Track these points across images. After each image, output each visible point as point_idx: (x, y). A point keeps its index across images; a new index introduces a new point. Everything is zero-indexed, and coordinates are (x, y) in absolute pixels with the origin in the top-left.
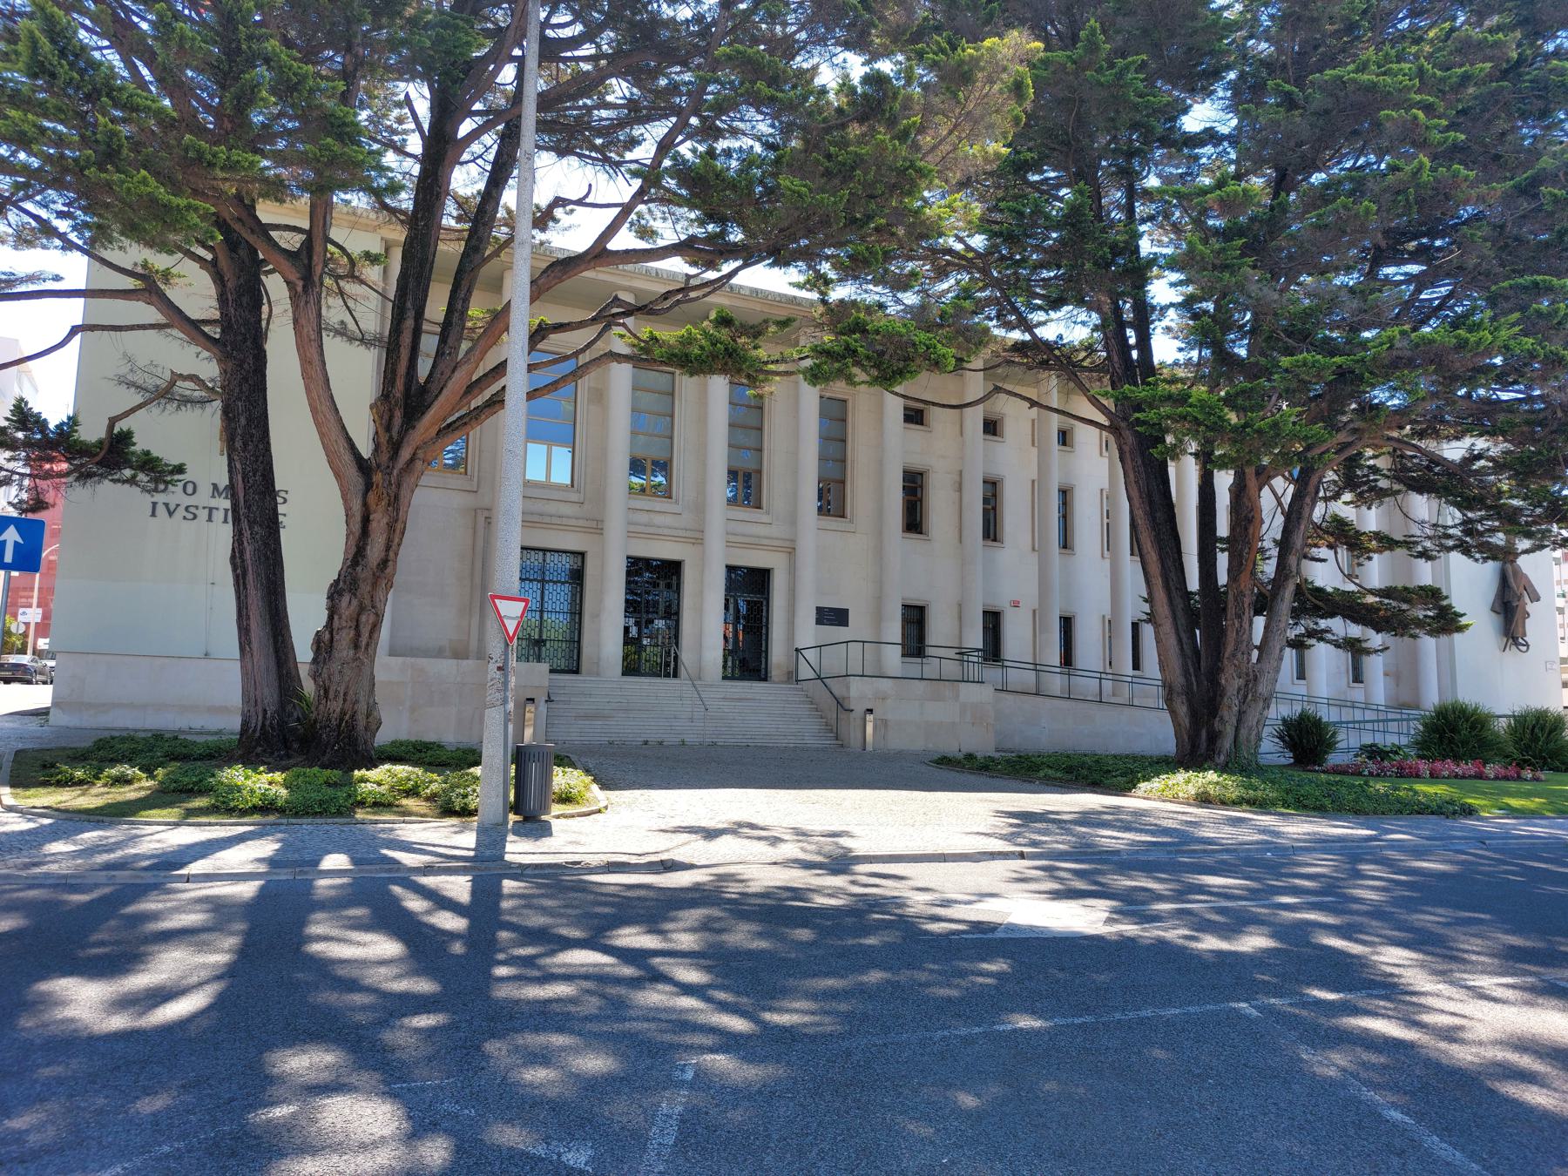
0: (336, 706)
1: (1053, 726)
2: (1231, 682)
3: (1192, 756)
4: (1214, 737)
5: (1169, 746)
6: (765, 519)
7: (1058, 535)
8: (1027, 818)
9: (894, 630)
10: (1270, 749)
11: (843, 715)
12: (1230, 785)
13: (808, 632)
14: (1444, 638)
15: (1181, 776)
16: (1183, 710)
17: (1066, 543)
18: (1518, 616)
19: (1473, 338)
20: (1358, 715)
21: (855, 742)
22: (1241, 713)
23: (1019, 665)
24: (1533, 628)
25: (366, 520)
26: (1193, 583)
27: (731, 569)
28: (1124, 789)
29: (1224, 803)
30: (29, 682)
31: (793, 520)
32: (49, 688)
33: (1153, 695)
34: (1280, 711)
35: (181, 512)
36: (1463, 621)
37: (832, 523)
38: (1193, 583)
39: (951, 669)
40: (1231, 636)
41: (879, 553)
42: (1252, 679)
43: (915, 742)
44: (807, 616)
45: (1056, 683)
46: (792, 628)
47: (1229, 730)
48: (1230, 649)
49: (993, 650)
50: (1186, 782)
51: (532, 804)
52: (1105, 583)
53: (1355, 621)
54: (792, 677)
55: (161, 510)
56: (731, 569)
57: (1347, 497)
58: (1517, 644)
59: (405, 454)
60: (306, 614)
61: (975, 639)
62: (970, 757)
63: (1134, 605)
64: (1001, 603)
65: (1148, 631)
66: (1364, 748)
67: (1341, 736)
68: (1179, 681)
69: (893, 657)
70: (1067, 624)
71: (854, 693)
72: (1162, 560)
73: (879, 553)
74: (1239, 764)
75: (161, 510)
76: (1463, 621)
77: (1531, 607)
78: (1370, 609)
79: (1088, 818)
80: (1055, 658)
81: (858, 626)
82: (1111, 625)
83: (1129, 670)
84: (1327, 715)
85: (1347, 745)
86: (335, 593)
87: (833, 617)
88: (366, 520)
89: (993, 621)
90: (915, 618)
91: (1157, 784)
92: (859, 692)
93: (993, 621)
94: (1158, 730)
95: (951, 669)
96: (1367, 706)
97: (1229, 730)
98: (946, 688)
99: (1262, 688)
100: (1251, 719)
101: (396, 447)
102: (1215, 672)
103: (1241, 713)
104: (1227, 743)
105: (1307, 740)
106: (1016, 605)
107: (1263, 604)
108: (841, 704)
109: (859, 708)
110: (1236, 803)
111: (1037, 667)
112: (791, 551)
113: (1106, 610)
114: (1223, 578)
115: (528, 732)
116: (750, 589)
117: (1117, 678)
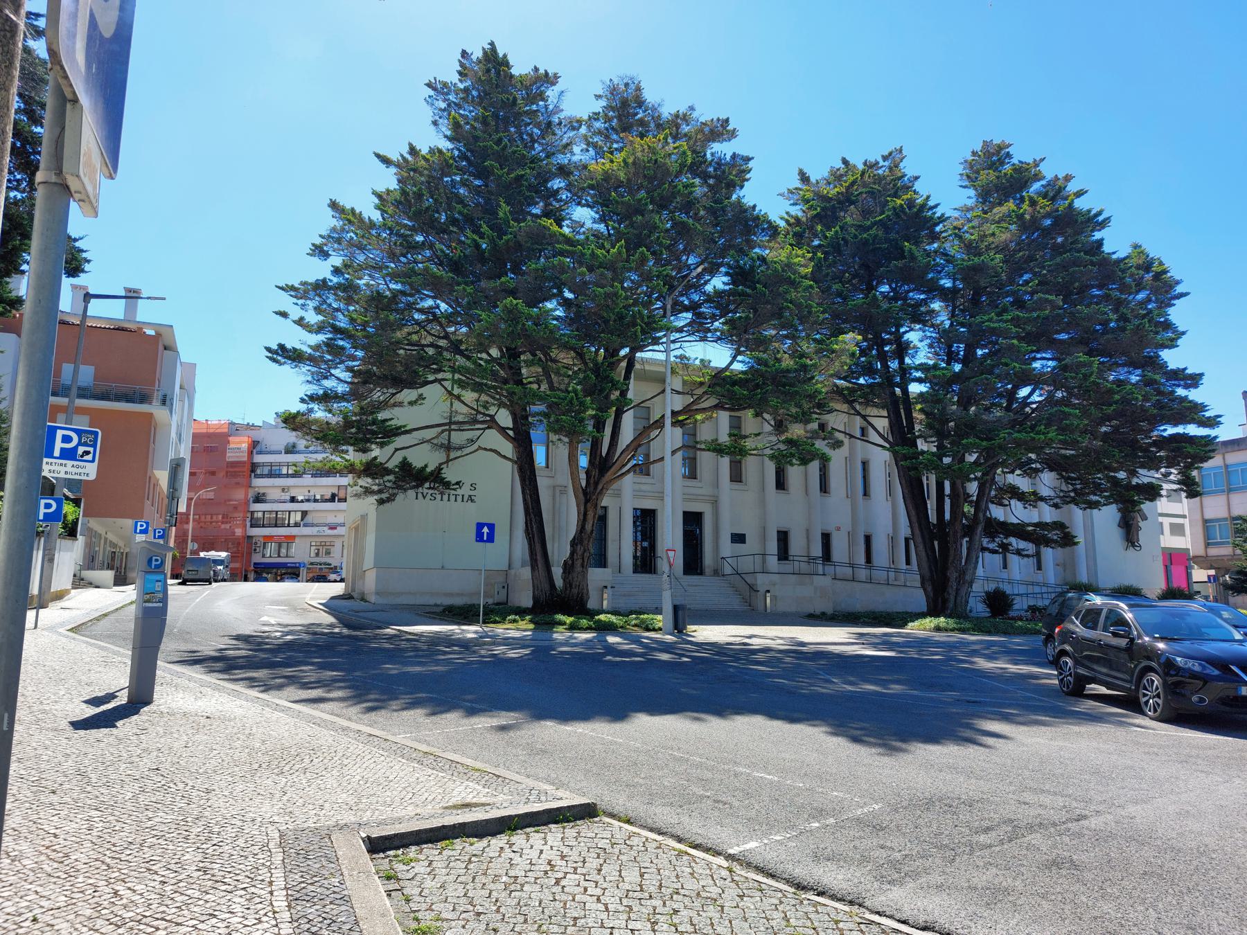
0: (575, 591)
1: (863, 597)
2: (953, 575)
3: (933, 612)
4: (945, 601)
5: (925, 609)
6: (699, 485)
7: (861, 491)
8: (862, 635)
9: (773, 546)
10: (978, 607)
11: (753, 593)
12: (951, 623)
13: (727, 548)
14: (1068, 549)
15: (928, 620)
16: (929, 589)
17: (866, 493)
18: (1133, 529)
19: (1037, 437)
20: (1037, 589)
21: (761, 608)
22: (957, 590)
23: (842, 564)
24: (1143, 537)
25: (585, 514)
26: (933, 518)
27: (685, 513)
28: (903, 626)
29: (946, 630)
30: (208, 581)
31: (716, 485)
32: (342, 585)
33: (916, 580)
34: (979, 588)
35: (429, 497)
36: (1076, 540)
37: (736, 486)
38: (933, 518)
39: (804, 567)
40: (952, 552)
41: (762, 502)
42: (963, 573)
43: (793, 609)
44: (726, 539)
45: (862, 574)
46: (717, 547)
47: (952, 598)
48: (951, 558)
49: (827, 555)
50: (929, 622)
51: (680, 626)
52: (887, 514)
53: (1025, 540)
54: (716, 572)
55: (420, 495)
56: (685, 513)
57: (1018, 472)
58: (1134, 546)
59: (600, 487)
60: (559, 551)
61: (817, 551)
62: (823, 614)
63: (904, 530)
64: (830, 528)
65: (912, 542)
66: (1030, 607)
67: (1017, 600)
68: (927, 574)
69: (773, 562)
70: (868, 539)
71: (759, 582)
72: (917, 514)
73: (762, 502)
74: (959, 614)
75: (420, 495)
76: (1076, 540)
77: (1141, 524)
78: (1028, 532)
79: (885, 635)
80: (861, 559)
81: (752, 545)
82: (893, 540)
83: (903, 565)
84: (1008, 589)
85: (1020, 605)
86: (574, 543)
87: (739, 538)
88: (585, 514)
89: (826, 538)
90: (783, 537)
91: (916, 623)
92: (761, 581)
93: (826, 538)
94: (919, 599)
95: (804, 567)
96: (1045, 585)
97: (952, 598)
98: (807, 579)
99: (968, 578)
100: (963, 592)
101: (596, 484)
102: (945, 568)
103: (957, 590)
104: (951, 605)
105: (998, 602)
106: (838, 529)
107: (969, 531)
108: (753, 588)
109: (762, 590)
110: (953, 630)
111: (852, 566)
112: (715, 503)
113: (890, 531)
114: (947, 516)
115: (605, 603)
116: (692, 521)
117: (897, 571)
